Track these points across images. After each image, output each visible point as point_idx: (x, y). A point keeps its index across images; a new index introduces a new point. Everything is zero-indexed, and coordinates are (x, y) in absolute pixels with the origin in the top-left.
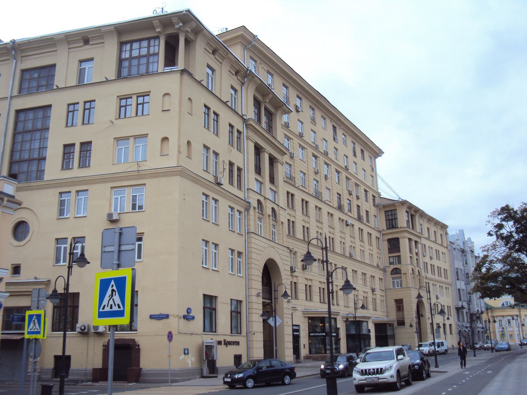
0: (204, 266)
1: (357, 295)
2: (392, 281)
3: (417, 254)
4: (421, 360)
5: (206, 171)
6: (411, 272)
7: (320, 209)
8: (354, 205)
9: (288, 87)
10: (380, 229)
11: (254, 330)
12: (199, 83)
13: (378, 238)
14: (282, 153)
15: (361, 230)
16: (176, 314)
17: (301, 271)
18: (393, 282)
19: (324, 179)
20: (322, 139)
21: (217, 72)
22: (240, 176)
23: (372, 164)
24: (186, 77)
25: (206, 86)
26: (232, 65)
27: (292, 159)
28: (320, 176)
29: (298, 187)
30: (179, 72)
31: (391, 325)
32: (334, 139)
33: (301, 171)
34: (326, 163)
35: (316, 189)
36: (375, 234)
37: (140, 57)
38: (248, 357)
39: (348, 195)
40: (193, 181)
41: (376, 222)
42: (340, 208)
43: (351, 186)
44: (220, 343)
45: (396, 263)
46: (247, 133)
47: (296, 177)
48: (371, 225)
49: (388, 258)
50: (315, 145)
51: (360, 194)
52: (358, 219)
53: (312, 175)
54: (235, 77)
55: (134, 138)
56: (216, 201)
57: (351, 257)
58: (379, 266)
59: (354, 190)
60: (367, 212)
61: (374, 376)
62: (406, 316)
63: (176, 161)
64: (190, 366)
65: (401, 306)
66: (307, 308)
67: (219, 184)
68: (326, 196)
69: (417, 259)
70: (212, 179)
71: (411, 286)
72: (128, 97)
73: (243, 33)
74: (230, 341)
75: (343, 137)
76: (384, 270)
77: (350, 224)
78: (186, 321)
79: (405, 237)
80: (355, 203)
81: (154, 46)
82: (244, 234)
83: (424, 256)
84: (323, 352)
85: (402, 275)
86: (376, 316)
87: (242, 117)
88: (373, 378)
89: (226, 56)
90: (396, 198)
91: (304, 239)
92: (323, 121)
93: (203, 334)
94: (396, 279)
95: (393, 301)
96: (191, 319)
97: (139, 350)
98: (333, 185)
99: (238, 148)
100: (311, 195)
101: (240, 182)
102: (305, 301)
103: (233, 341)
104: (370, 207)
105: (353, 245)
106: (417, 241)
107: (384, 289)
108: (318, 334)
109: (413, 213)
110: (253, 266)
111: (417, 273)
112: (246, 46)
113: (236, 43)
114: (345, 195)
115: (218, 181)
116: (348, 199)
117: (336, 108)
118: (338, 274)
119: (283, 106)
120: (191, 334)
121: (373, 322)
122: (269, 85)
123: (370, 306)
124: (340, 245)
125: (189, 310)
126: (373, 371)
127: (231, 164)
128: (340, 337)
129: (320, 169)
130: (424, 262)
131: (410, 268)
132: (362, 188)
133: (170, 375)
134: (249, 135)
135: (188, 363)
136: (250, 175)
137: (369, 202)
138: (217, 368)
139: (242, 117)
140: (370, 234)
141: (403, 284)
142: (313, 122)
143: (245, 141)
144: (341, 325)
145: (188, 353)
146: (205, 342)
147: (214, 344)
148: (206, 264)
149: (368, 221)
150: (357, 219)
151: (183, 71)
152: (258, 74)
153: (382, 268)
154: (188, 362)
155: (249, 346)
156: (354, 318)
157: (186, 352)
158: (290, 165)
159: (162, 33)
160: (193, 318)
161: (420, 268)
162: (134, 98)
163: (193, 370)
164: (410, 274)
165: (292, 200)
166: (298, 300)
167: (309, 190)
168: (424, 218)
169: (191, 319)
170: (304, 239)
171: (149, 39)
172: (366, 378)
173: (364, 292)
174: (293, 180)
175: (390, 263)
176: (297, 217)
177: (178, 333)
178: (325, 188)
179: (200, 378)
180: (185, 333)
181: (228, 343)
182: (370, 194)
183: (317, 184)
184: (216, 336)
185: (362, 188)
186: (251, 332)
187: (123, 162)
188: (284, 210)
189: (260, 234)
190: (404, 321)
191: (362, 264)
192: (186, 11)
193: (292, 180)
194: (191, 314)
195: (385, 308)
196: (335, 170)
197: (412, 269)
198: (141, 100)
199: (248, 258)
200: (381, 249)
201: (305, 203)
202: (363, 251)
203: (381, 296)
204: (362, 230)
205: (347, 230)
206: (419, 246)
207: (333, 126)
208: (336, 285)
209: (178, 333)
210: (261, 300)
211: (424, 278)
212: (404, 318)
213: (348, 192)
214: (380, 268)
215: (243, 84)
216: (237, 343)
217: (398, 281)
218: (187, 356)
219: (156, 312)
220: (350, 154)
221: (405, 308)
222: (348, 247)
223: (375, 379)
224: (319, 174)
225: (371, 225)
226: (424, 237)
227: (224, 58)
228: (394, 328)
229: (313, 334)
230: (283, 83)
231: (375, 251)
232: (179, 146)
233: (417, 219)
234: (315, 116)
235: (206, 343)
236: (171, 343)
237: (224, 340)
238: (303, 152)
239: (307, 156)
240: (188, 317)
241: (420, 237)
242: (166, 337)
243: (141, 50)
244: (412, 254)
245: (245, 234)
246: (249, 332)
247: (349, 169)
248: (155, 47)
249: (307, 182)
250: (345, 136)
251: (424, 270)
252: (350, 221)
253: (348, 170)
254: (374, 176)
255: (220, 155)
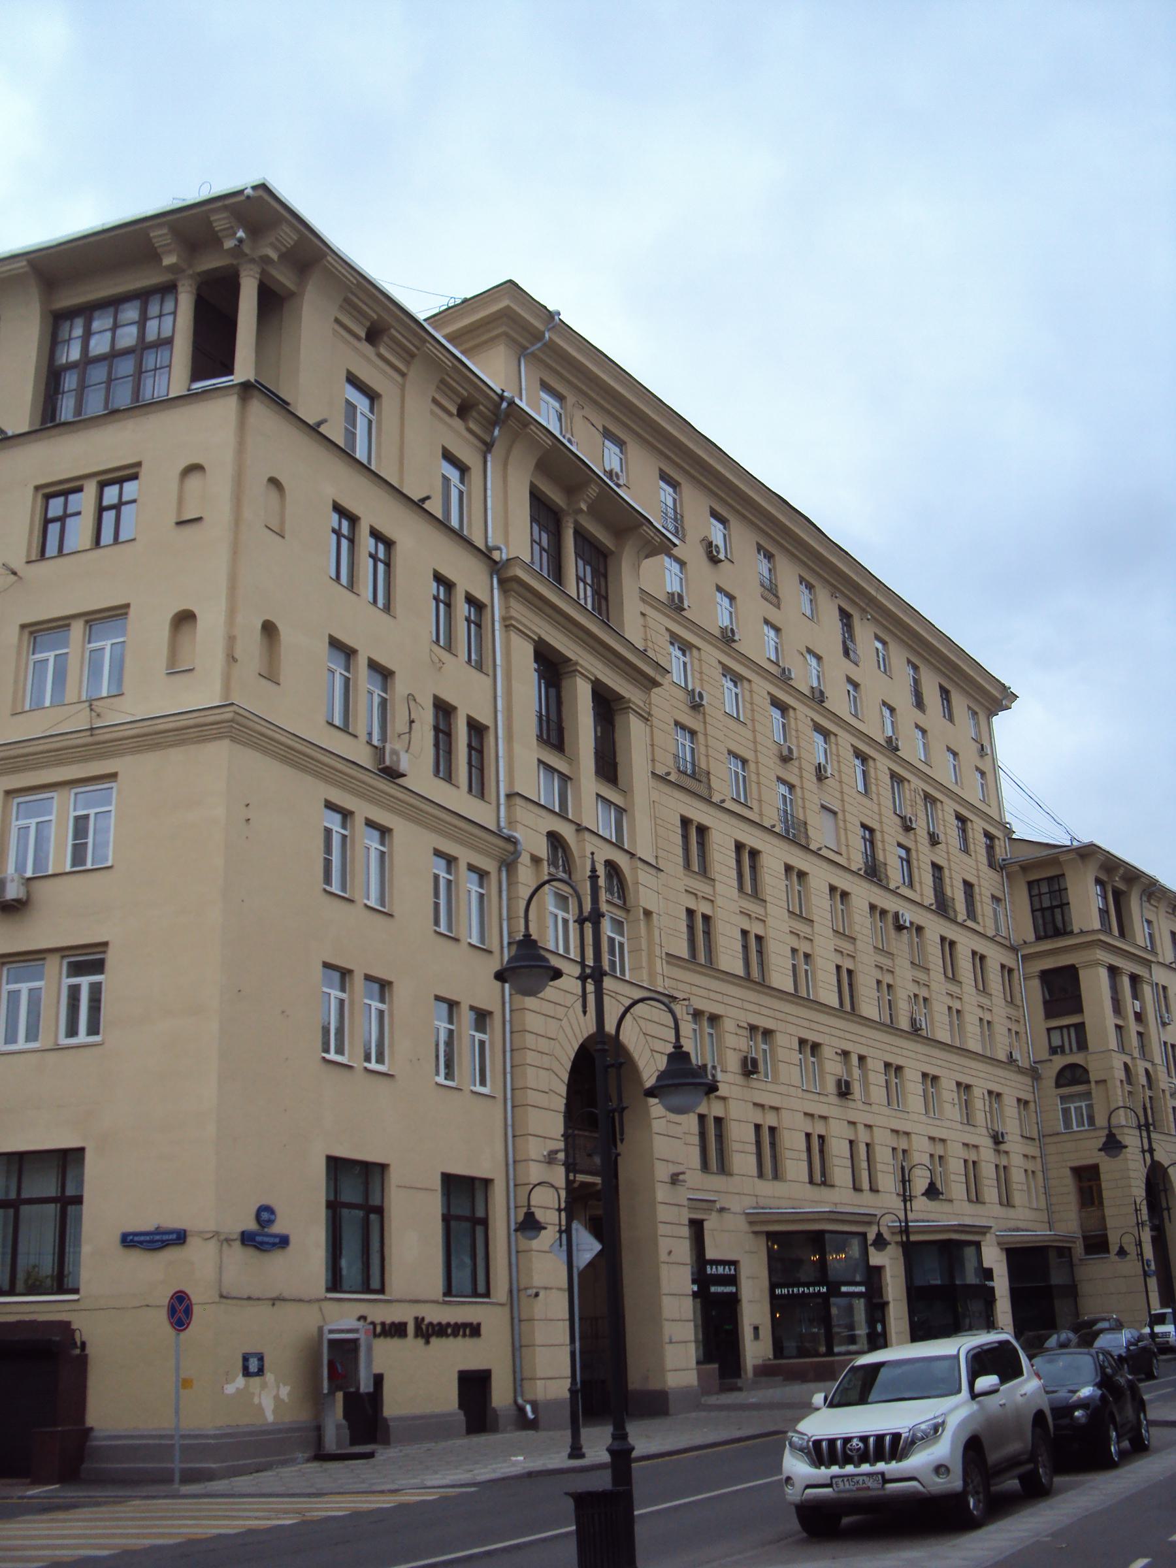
0: (332, 1056)
1: (941, 1157)
2: (1060, 1107)
3: (1139, 1017)
4: (1099, 1385)
5: (345, 729)
6: (1120, 1074)
7: (802, 875)
8: (922, 865)
9: (679, 484)
10: (1016, 939)
11: (538, 1280)
12: (313, 430)
13: (1010, 971)
14: (646, 683)
15: (948, 945)
16: (212, 1227)
17: (739, 1079)
18: (1066, 1112)
19: (814, 779)
20: (804, 651)
21: (388, 404)
22: (481, 752)
23: (978, 733)
24: (258, 409)
25: (343, 446)
26: (443, 381)
27: (699, 712)
28: (800, 768)
29: (898, 891)
30: (236, 390)
31: (1064, 1252)
32: (846, 653)
33: (730, 752)
34: (818, 728)
35: (785, 812)
36: (996, 957)
37: (114, 355)
38: (518, 1376)
39: (900, 830)
40: (284, 760)
41: (1002, 918)
42: (873, 872)
43: (911, 800)
44: (397, 1330)
45: (1071, 1049)
46: (508, 608)
47: (711, 771)
48: (984, 927)
49: (1046, 1032)
50: (780, 670)
51: (942, 828)
52: (938, 908)
53: (769, 767)
54: (457, 423)
55: (87, 622)
56: (384, 832)
57: (915, 1031)
58: (1015, 1061)
59: (922, 815)
60: (968, 886)
61: (866, 1468)
62: (1110, 1223)
63: (217, 686)
64: (270, 1418)
65: (1094, 1188)
66: (762, 1202)
67: (392, 774)
68: (821, 833)
69: (1140, 1034)
70: (363, 756)
71: (1124, 1123)
72: (68, 489)
73: (512, 305)
74: (439, 1324)
75: (879, 645)
76: (1034, 1073)
77: (908, 924)
78: (251, 1252)
79: (1097, 963)
80: (924, 856)
81: (160, 316)
82: (495, 947)
83: (1164, 1024)
84: (823, 1349)
85: (1093, 1085)
86: (1012, 1224)
87: (485, 555)
88: (861, 1478)
89: (418, 349)
90: (1059, 838)
91: (748, 973)
92: (805, 596)
93: (326, 1299)
94: (1073, 1102)
95: (1068, 1172)
96: (274, 1245)
97: (82, 1363)
98: (846, 798)
99: (473, 657)
100: (770, 830)
101: (481, 770)
102: (756, 1180)
103: (452, 1322)
104: (978, 870)
105: (923, 993)
106: (1118, 968)
107: (1036, 1136)
108: (801, 1290)
109: (1122, 886)
110: (531, 1057)
111: (1143, 1080)
112: (526, 348)
113: (492, 339)
114: (890, 832)
115: (388, 763)
116: (900, 845)
117: (847, 553)
118: (872, 1087)
119: (643, 524)
120: (275, 1301)
121: (999, 1244)
122: (610, 474)
123: (957, 1189)
124: (875, 994)
125: (265, 1214)
126: (861, 1445)
127: (444, 710)
128: (885, 1299)
129: (798, 746)
130: (1165, 1043)
131: (1118, 1061)
132: (949, 808)
133: (177, 1453)
134: (513, 613)
135: (260, 1408)
136: (517, 747)
137: (973, 854)
138: (385, 1420)
139: (485, 555)
140: (979, 959)
141: (1096, 1117)
142: (771, 597)
143: (497, 633)
144: (993, 1258)
145: (260, 1372)
146: (326, 1329)
147: (361, 1336)
148: (340, 1051)
149: (971, 913)
150: (933, 907)
151: (247, 389)
152: (568, 436)
153: (1028, 1067)
154: (260, 1405)
155: (520, 1340)
156: (901, 1232)
157: (253, 1365)
158: (693, 733)
159: (183, 271)
160: (283, 1242)
161: (1153, 1064)
162: (91, 488)
163: (280, 1431)
164: (1118, 1083)
165: (754, 868)
166: (729, 1178)
167: (761, 815)
168: (1159, 900)
169: (274, 1245)
170: (748, 973)
171: (143, 296)
172: (832, 1477)
173: (966, 1145)
174: (704, 779)
175: (1054, 1051)
176: (719, 901)
177: (217, 1296)
178: (817, 808)
179: (308, 1460)
180: (249, 1298)
181: (428, 1331)
182: (977, 827)
183: (790, 793)
184: (381, 1305)
185: (946, 808)
186: (526, 1289)
187: (47, 704)
188: (653, 871)
189: (561, 951)
190: (1106, 1236)
191: (957, 1054)
192: (254, 188)
193: (700, 781)
194: (277, 1228)
195: (1043, 1197)
196: (851, 749)
197: (1126, 1065)
198: (111, 495)
199: (512, 1033)
200: (1019, 1003)
201: (747, 856)
202: (958, 1011)
203: (1025, 1156)
204: (952, 944)
205: (901, 944)
206: (1147, 990)
207: (841, 610)
208: (866, 1125)
209: (217, 1299)
210: (558, 1175)
211: (1168, 1096)
212: (1106, 1229)
213: (898, 820)
214: (1018, 1066)
215: (487, 447)
216: (474, 1330)
217: (1081, 1107)
218: (256, 1380)
219: (144, 1223)
220: (903, 700)
221: (1105, 1194)
222: (906, 998)
223: (870, 1483)
224: (796, 763)
225: (984, 927)
226: (1159, 963)
227: (413, 356)
228: (1075, 1261)
229: (785, 1291)
230: (661, 470)
231: (1000, 1012)
232: (230, 637)
233: (1135, 905)
234: (776, 579)
235: (331, 1331)
236: (182, 1335)
237: (416, 1319)
238: (687, 660)
239: (701, 673)
240: (259, 1239)
241: (1147, 963)
242: (163, 1314)
243: (119, 332)
244: (1124, 1018)
245: (502, 948)
246: (519, 1291)
247: (793, 676)
248: (163, 319)
249: (754, 786)
250: (884, 643)
251: (1165, 1070)
252: (909, 915)
253: (898, 750)
254: (987, 771)
255: (397, 675)
